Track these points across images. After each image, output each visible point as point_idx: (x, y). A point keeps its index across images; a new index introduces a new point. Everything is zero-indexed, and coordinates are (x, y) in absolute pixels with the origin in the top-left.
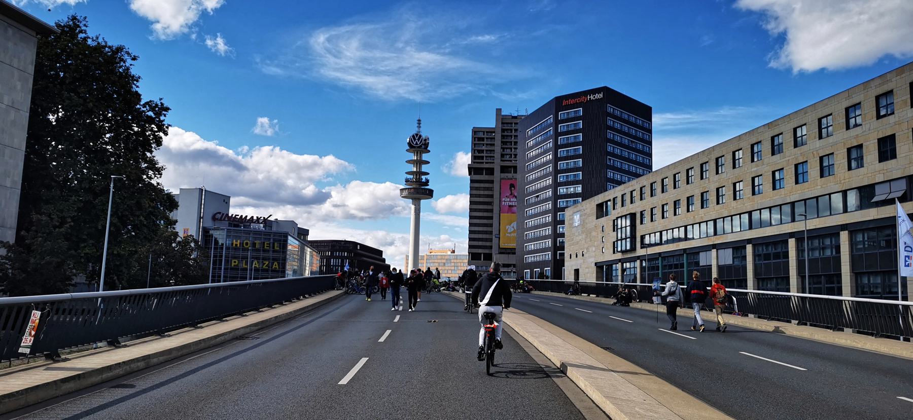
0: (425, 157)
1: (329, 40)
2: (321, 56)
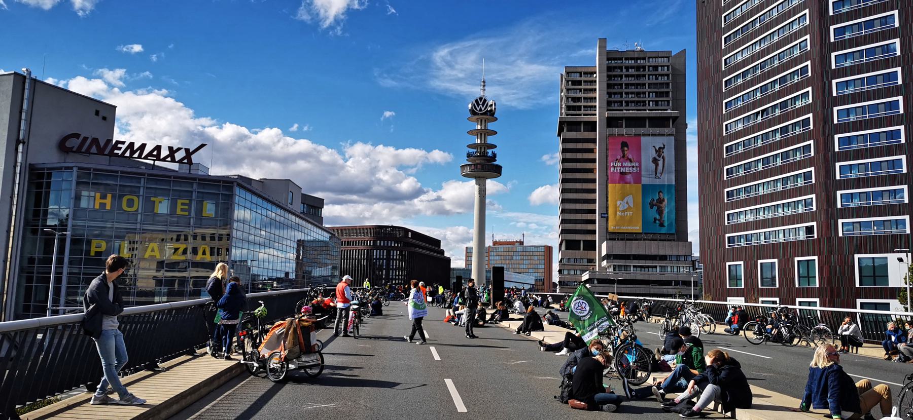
0: (491, 126)
1: (451, 53)
2: (440, 69)
